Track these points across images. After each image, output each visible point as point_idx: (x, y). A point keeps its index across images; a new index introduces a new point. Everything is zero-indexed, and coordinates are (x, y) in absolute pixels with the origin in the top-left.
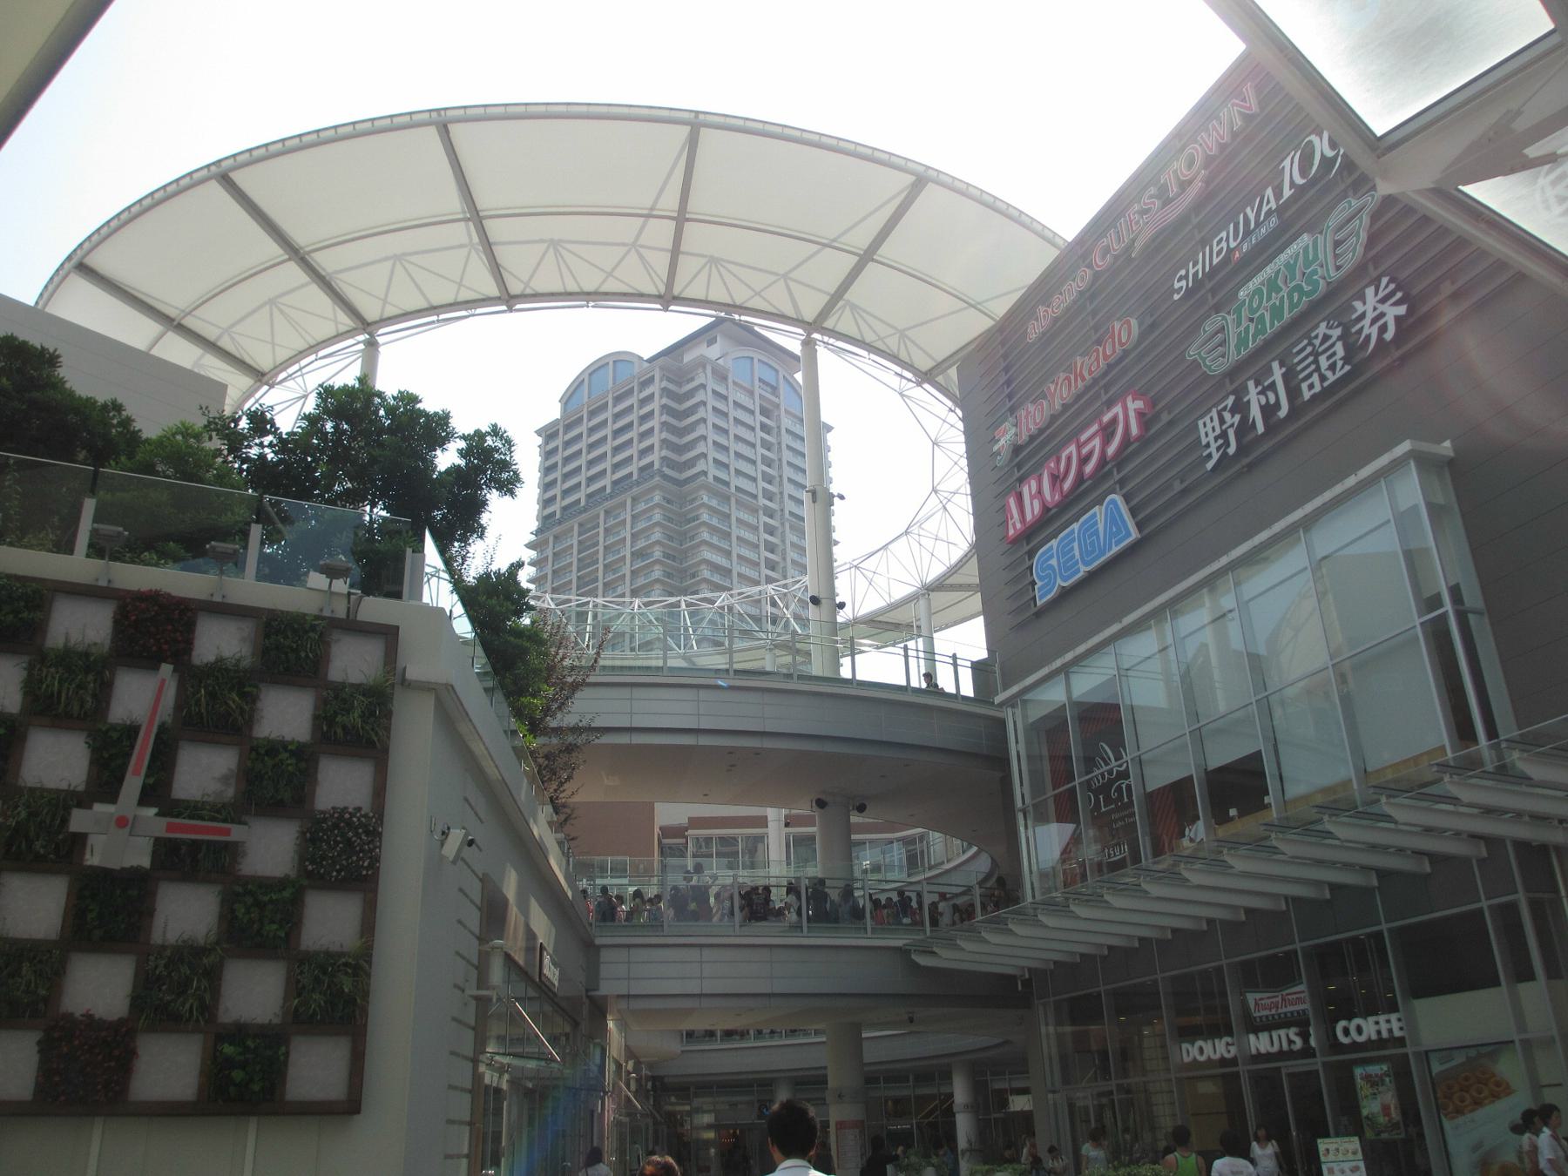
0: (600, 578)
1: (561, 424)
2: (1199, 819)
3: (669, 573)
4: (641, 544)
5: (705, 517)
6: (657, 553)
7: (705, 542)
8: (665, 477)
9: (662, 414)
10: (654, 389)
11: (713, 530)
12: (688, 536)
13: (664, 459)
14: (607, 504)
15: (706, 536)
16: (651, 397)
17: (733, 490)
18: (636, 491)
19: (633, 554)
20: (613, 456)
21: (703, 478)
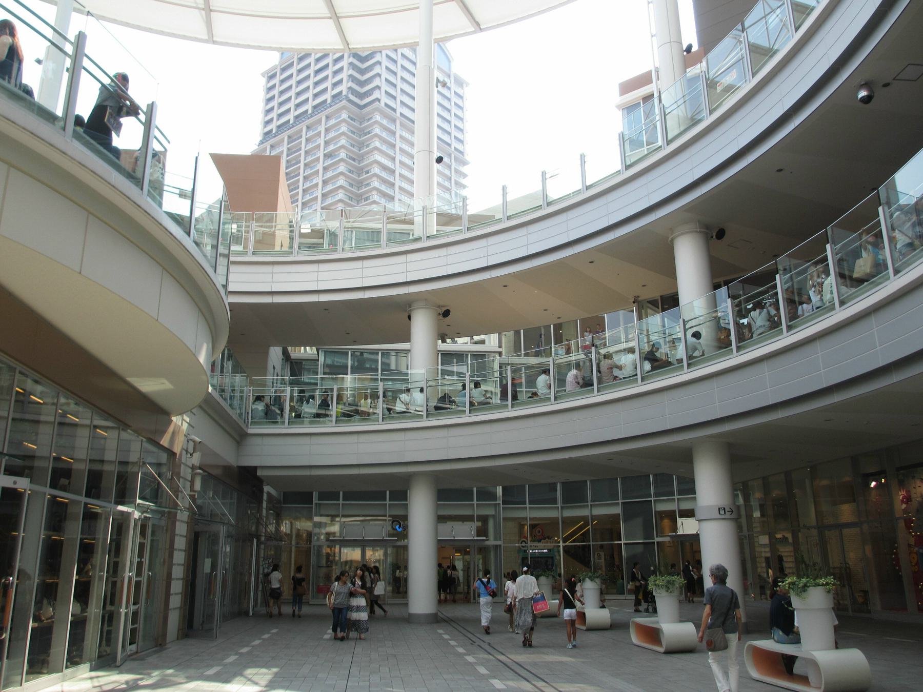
0: (303, 146)
1: (279, 68)
2: (739, 607)
3: (349, 197)
4: (331, 148)
5: (377, 130)
6: (343, 154)
7: (376, 148)
8: (350, 101)
9: (349, 69)
10: (344, 63)
11: (384, 141)
12: (364, 197)
13: (350, 88)
14: (308, 122)
15: (377, 144)
16: (341, 81)
17: (398, 114)
18: (329, 111)
19: (325, 155)
20: (314, 100)
21: (377, 103)
